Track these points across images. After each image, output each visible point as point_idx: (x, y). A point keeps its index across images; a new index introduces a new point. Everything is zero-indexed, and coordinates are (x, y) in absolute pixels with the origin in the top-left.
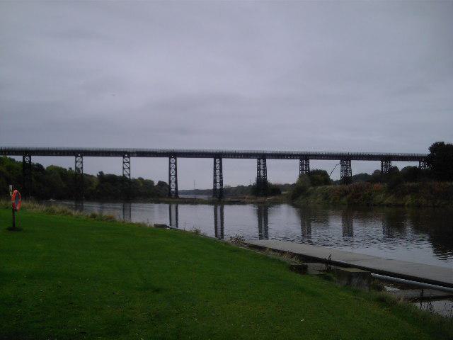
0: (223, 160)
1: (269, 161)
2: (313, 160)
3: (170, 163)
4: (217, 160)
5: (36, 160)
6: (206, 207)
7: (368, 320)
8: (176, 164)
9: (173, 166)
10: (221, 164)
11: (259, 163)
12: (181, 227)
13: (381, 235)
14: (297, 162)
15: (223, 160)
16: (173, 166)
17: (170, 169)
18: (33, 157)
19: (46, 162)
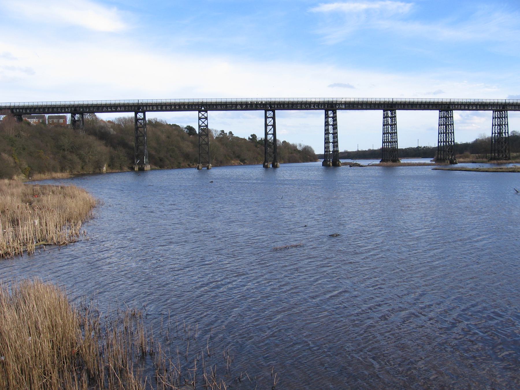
0: (339, 113)
1: (340, 114)
2: (398, 111)
3: (266, 118)
4: (270, 114)
5: (150, 116)
6: (352, 148)
7: (126, 305)
8: (274, 118)
9: (270, 121)
10: (335, 119)
11: (327, 116)
12: (399, 148)
13: (93, 305)
14: (379, 114)
15: (339, 113)
16: (270, 121)
17: (266, 125)
18: (147, 113)
19: (104, 117)
